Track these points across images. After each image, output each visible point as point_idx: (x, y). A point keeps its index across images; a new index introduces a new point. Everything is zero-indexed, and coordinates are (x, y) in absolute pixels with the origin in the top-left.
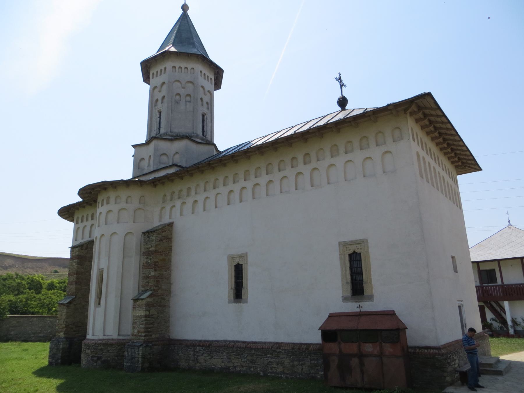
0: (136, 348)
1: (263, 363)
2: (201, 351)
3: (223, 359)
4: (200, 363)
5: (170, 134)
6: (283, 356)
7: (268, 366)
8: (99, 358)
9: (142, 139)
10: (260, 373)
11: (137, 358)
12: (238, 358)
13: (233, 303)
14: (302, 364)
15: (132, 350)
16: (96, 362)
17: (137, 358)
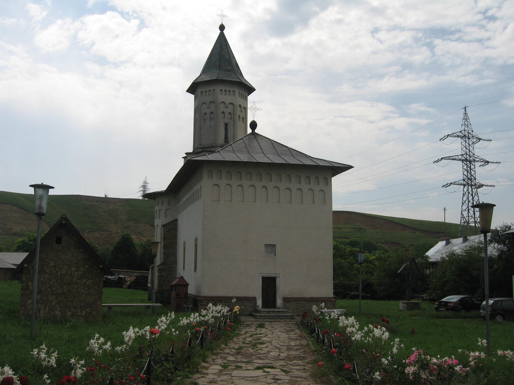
5: (200, 147)
9: (191, 150)
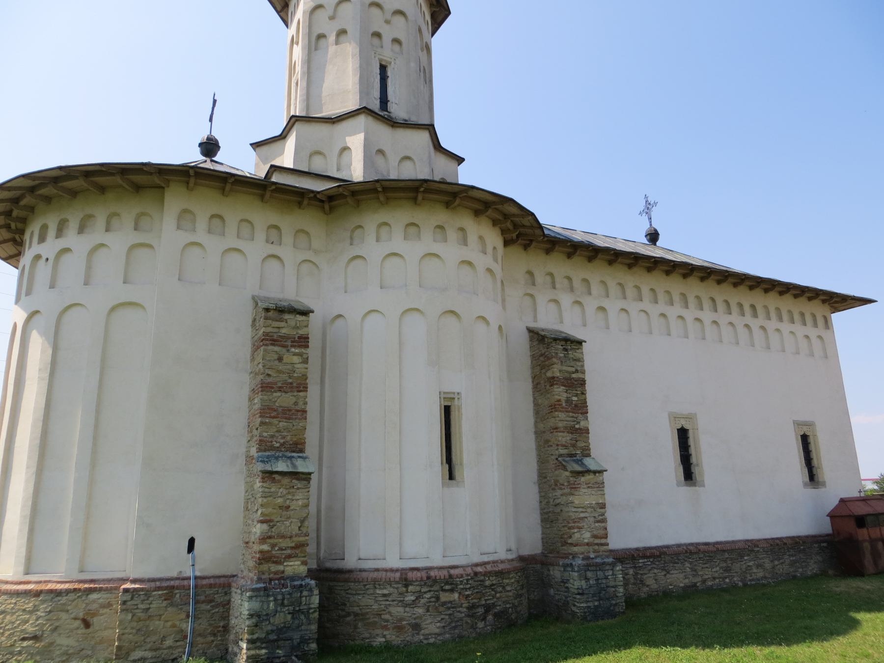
0: (607, 567)
1: (741, 569)
2: (646, 565)
3: (685, 572)
4: (648, 586)
6: (763, 556)
7: (747, 571)
8: (488, 608)
10: (738, 584)
11: (613, 587)
12: (707, 567)
13: (684, 486)
14: (782, 563)
15: (598, 573)
16: (484, 619)
17: (613, 587)
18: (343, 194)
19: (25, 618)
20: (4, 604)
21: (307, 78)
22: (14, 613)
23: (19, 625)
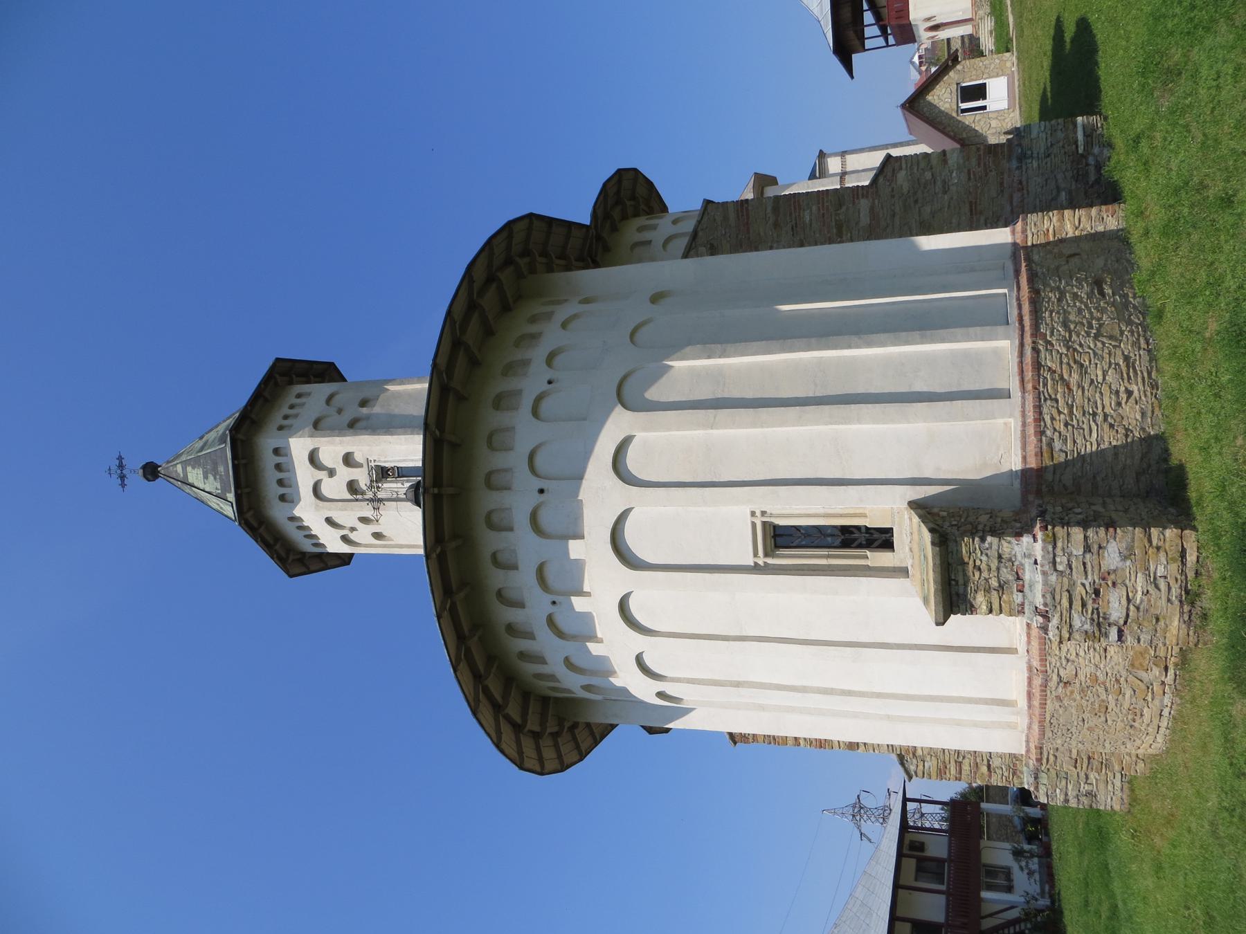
18: (449, 609)
19: (1070, 297)
20: (1053, 325)
21: (236, 468)
22: (1064, 310)
23: (1081, 302)
